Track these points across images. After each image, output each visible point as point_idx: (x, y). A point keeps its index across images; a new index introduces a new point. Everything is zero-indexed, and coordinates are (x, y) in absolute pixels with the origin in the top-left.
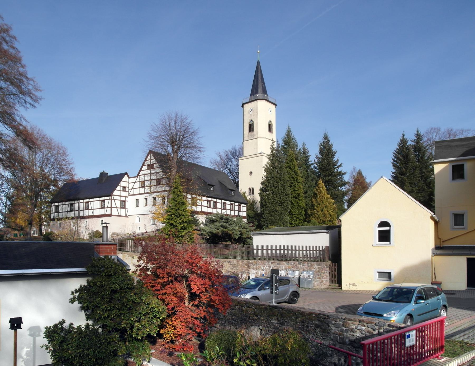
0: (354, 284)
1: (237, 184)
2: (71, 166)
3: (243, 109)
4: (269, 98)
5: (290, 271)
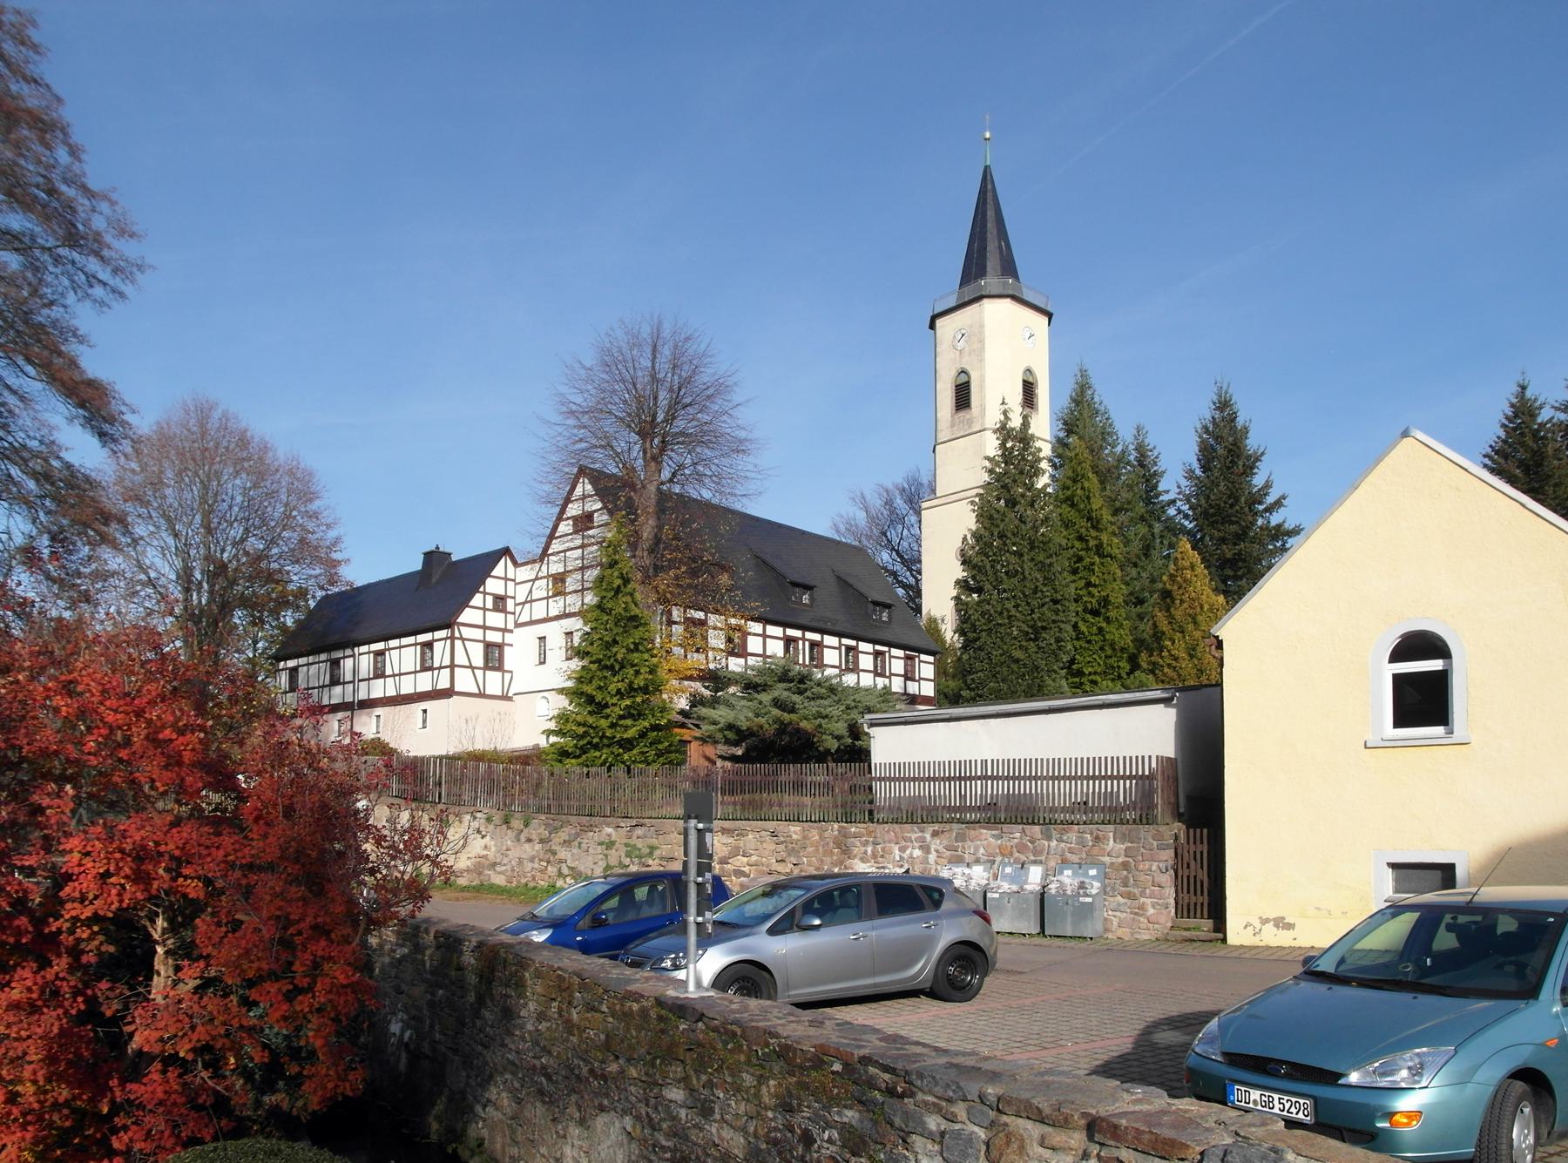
0: (1283, 918)
1: (915, 592)
2: (332, 534)
3: (935, 333)
4: (1024, 290)
5: (1005, 865)
